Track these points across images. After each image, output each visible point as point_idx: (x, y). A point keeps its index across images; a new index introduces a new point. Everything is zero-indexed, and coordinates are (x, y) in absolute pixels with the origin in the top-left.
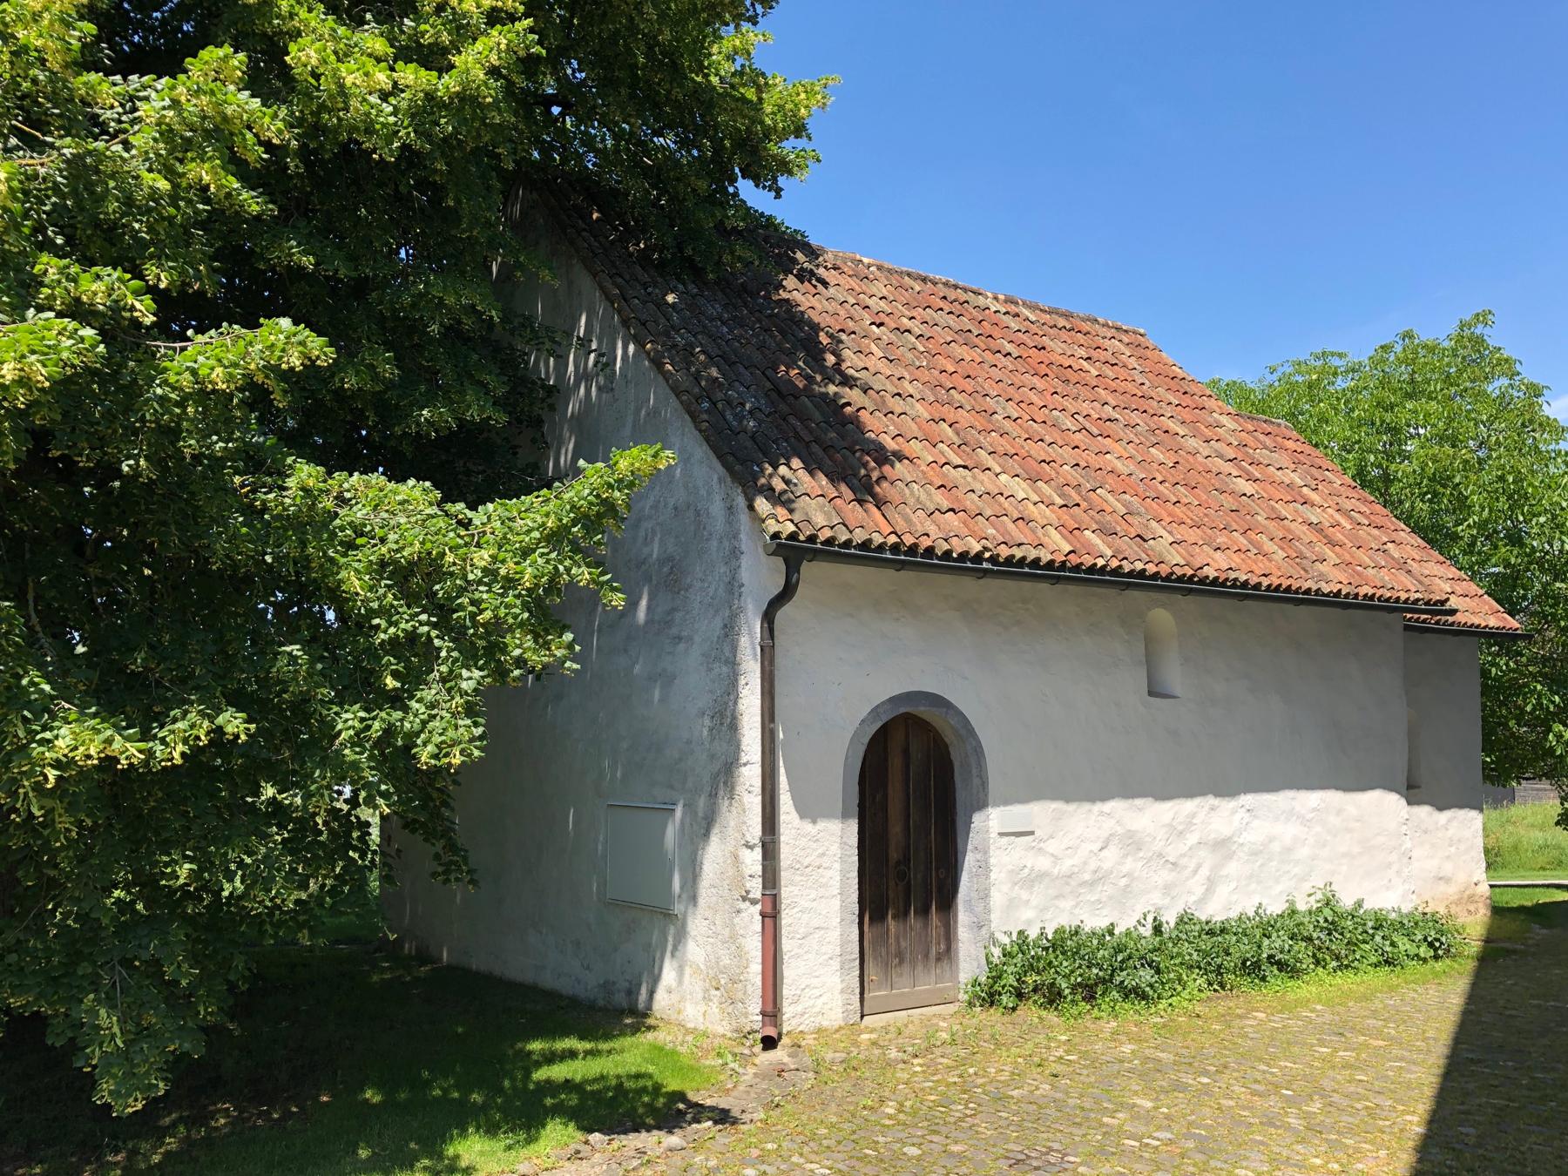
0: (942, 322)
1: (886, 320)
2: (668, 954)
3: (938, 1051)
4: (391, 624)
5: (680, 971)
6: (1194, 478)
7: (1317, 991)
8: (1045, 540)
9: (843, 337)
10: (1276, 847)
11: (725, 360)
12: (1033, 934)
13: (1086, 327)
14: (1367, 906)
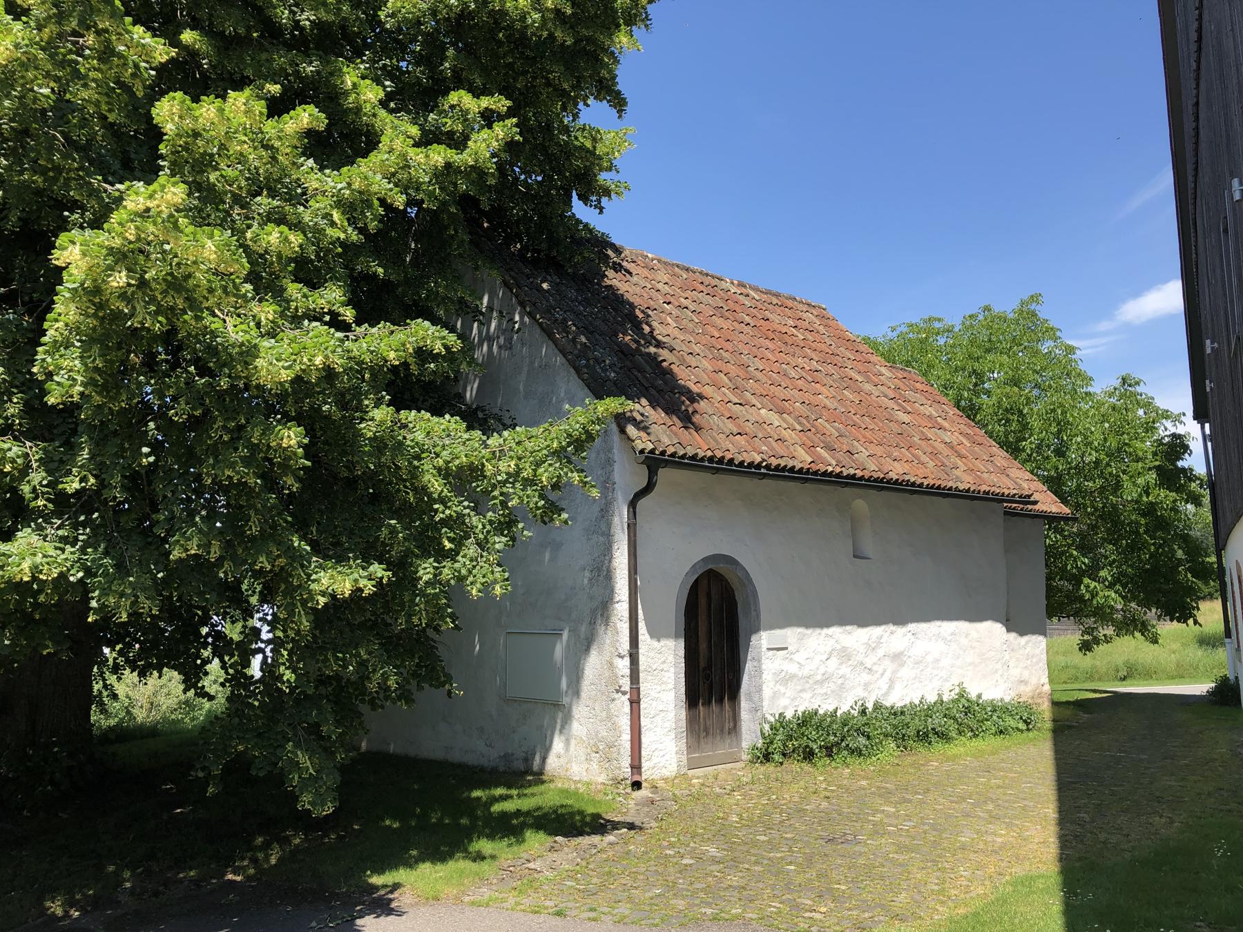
0: (704, 300)
1: (672, 300)
2: (557, 732)
3: (747, 788)
4: (447, 507)
5: (567, 742)
6: (874, 412)
7: (963, 749)
8: (795, 454)
9: (650, 312)
10: (929, 659)
11: (588, 330)
12: (789, 715)
13: (790, 303)
14: (984, 697)
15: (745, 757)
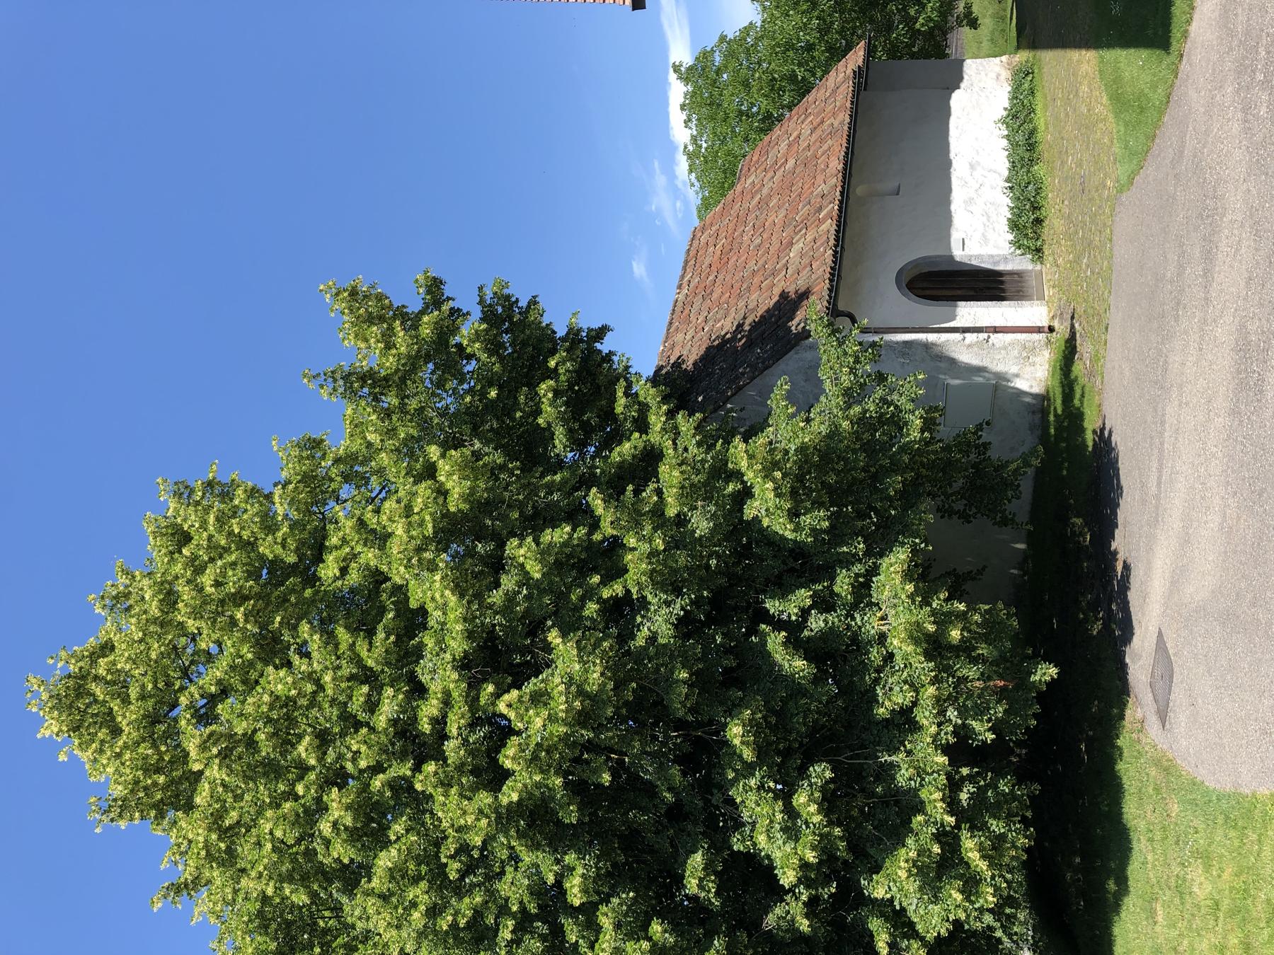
7: (1041, 119)
12: (1011, 237)
13: (692, 253)
15: (1038, 267)
